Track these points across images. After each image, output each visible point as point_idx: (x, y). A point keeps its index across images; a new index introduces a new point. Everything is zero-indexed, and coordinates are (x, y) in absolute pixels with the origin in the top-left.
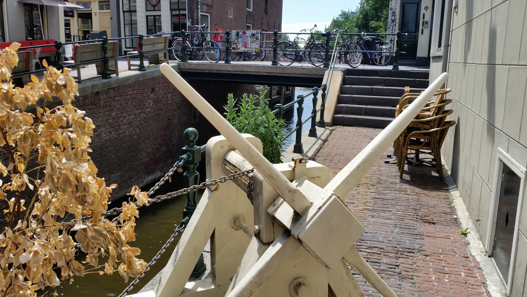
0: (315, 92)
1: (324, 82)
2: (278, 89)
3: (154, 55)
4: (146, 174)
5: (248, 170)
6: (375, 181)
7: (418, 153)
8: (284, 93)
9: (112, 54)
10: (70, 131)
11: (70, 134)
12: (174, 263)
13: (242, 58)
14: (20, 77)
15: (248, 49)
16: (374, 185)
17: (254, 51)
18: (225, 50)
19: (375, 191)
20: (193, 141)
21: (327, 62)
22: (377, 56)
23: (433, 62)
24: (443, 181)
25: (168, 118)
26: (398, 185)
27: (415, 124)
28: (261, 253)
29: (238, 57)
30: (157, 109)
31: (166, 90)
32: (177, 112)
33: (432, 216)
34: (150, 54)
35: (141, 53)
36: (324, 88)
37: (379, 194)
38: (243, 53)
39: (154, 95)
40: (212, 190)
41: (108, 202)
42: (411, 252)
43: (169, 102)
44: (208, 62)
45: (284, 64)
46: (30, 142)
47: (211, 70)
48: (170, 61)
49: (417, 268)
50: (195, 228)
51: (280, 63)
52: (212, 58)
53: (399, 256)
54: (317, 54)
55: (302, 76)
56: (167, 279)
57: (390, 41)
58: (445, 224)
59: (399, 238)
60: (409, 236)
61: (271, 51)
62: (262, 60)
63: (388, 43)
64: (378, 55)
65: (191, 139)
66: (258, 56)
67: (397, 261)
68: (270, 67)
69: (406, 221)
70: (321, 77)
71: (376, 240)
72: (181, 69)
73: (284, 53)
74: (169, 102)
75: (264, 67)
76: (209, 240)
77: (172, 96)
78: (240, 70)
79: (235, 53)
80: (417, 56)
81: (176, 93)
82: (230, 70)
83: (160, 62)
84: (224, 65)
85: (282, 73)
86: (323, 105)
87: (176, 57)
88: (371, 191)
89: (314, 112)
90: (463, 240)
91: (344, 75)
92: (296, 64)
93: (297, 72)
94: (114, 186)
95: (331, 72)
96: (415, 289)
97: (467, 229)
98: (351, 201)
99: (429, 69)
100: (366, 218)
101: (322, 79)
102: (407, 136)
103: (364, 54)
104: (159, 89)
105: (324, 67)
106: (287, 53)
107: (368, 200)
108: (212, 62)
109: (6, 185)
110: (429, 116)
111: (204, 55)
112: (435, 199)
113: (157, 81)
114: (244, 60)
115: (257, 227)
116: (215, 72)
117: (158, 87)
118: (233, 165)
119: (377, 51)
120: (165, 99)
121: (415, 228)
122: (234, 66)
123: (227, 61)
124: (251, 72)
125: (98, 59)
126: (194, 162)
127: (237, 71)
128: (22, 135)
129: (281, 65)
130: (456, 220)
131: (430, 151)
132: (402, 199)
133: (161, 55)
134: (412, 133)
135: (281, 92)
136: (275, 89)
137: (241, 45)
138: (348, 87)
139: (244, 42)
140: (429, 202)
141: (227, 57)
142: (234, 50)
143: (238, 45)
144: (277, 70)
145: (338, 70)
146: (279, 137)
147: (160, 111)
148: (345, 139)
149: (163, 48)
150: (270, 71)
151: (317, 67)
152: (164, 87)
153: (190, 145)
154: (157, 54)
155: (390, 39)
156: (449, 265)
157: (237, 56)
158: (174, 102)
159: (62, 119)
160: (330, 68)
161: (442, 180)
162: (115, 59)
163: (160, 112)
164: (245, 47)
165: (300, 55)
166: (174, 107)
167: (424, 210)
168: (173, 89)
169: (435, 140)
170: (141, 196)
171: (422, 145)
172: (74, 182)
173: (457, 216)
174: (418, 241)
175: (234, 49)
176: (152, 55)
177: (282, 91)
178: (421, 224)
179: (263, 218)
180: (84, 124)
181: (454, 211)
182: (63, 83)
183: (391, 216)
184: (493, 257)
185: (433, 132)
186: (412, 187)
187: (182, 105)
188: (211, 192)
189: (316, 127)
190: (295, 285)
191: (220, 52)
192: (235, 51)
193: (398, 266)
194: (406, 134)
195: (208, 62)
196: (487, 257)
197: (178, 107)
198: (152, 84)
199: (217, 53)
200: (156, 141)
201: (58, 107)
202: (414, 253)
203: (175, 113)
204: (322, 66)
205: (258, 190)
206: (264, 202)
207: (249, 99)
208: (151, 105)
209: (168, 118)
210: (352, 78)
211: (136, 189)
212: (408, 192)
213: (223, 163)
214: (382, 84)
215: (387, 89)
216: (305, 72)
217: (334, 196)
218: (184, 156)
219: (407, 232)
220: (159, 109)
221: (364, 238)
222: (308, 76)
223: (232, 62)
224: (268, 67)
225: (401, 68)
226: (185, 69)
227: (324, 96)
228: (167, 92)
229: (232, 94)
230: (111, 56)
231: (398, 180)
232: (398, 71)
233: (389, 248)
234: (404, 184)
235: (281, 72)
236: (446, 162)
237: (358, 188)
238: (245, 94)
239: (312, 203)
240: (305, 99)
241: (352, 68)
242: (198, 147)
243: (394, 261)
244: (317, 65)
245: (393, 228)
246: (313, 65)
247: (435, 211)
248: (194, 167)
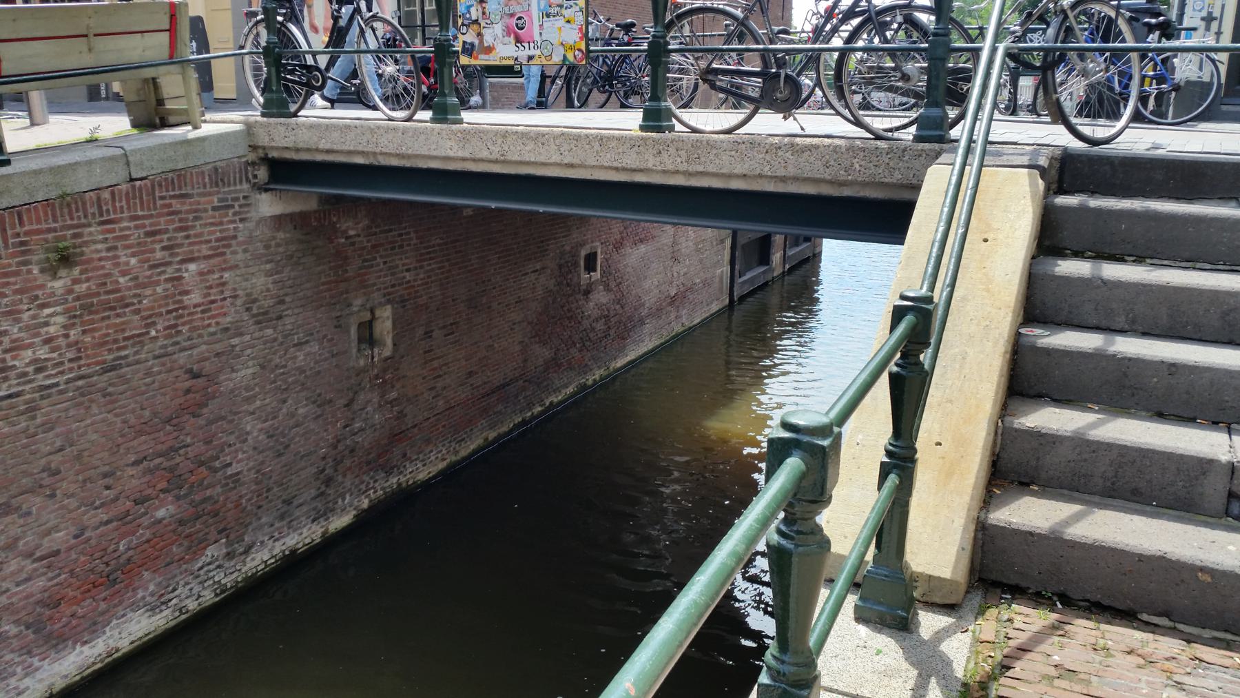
4: (36, 651)
15: (532, 52)
21: (935, 112)
43: (195, 298)
47: (375, 154)
51: (868, 120)
54: (880, 69)
55: (792, 188)
57: (1203, 19)
63: (1194, 29)
70: (906, 195)
72: (264, 148)
73: (703, 64)
75: (602, 140)
78: (493, 157)
82: (451, 154)
92: (768, 123)
93: (767, 170)
105: (918, 139)
113: (95, 210)
120: (159, 289)
124: (544, 164)
127: (482, 160)
137: (498, 29)
139: (512, 15)
142: (471, 55)
143: (483, 31)
144: (665, 155)
145: (1004, 160)
149: (164, 54)
150: (631, 160)
155: (1204, 14)
163: (123, 353)
164: (518, 40)
165: (787, 76)
175: (469, 50)
192: (473, 62)
197: (254, 316)
200: (108, 488)
203: (235, 341)
209: (190, 371)
223: (466, 116)
226: (277, 148)
246: (858, 123)
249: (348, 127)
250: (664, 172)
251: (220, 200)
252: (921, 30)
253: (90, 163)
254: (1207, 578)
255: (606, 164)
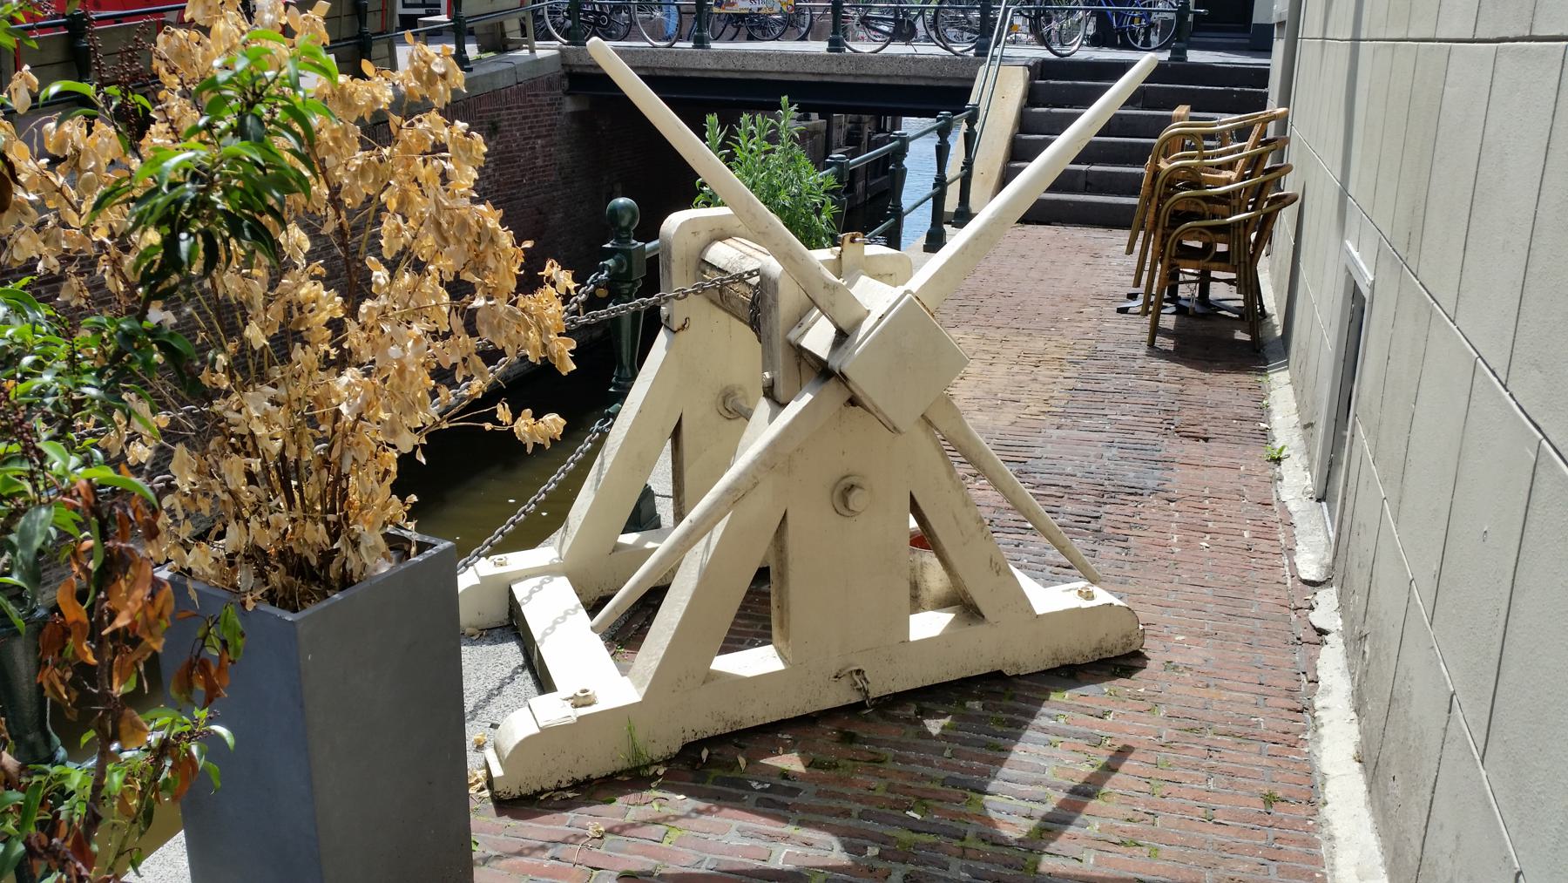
0: (943, 125)
1: (973, 100)
2: (849, 126)
3: (492, 25)
5: (750, 270)
6: (1083, 352)
7: (1205, 281)
8: (870, 137)
9: (380, 26)
10: (443, 158)
11: (443, 162)
12: (597, 484)
13: (744, 31)
14: (501, 19)
15: (761, 6)
16: (1077, 363)
17: (776, 10)
18: (694, 9)
19: (1076, 375)
20: (627, 229)
22: (1137, 20)
23: (1278, 38)
24: (1258, 351)
25: (537, 209)
26: (1139, 361)
27: (1192, 202)
28: (772, 419)
29: (731, 30)
30: (506, 184)
31: (529, 128)
32: (560, 193)
33: (1205, 426)
34: (480, 22)
35: (459, 20)
36: (970, 115)
37: (1086, 380)
38: (746, 15)
39: (498, 143)
40: (675, 329)
41: (520, 270)
42: (1135, 494)
44: (647, 44)
45: (864, 47)
46: (372, 177)
47: (653, 68)
48: (537, 43)
49: (1143, 522)
50: (640, 411)
51: (851, 46)
52: (657, 32)
53: (1105, 500)
54: (957, 18)
56: (582, 518)
58: (1233, 441)
59: (1112, 467)
60: (1139, 463)
61: (826, 9)
62: (803, 38)
64: (1141, 17)
65: (624, 223)
66: (790, 25)
67: (1098, 509)
68: (823, 56)
69: (1138, 435)
71: (1056, 471)
72: (570, 66)
74: (539, 162)
75: (806, 57)
76: (669, 441)
77: (546, 146)
78: (736, 68)
79: (722, 17)
80: (1254, 22)
81: (558, 138)
82: (709, 67)
83: (510, 46)
84: (691, 53)
85: (856, 76)
86: (968, 165)
87: (553, 31)
88: (1066, 375)
89: (941, 183)
90: (1270, 473)
91: (1032, 77)
92: (897, 49)
94: (528, 244)
95: (993, 69)
96: (1127, 558)
97: (1283, 447)
98: (1013, 397)
99: (1270, 57)
100: (1043, 430)
101: (970, 90)
102: (1169, 236)
103: (1102, 18)
104: (510, 125)
105: (976, 55)
106: (874, 13)
107: (1055, 394)
108: (655, 43)
109: (314, 264)
110: (1229, 182)
111: (632, 23)
112: (1225, 390)
114: (751, 38)
115: (767, 375)
116: (667, 73)
117: (508, 120)
118: (720, 270)
119: (1137, 5)
121: (1158, 448)
122: (721, 55)
123: (700, 42)
124: (770, 72)
125: (345, 40)
126: (631, 276)
127: (729, 71)
128: (358, 165)
129: (855, 51)
130: (1264, 433)
131: (1233, 276)
132: (1140, 390)
133: (512, 27)
134: (1183, 227)
135: (857, 134)
136: (841, 127)
138: (1042, 113)
140: (1208, 397)
141: (700, 30)
146: (823, 217)
147: (513, 188)
148: (1023, 256)
150: (823, 68)
151: (956, 55)
152: (524, 118)
153: (621, 238)
154: (502, 24)
156: (1219, 518)
157: (729, 26)
158: (553, 162)
159: (426, 139)
160: (989, 58)
161: (1257, 348)
162: (388, 40)
165: (909, 21)
166: (553, 178)
167: (1190, 413)
168: (550, 125)
169: (1242, 243)
170: (562, 277)
171: (1209, 258)
172: (475, 228)
173: (1269, 424)
174: (1157, 473)
176: (486, 27)
177: (862, 133)
178: (1172, 440)
179: (780, 354)
180: (470, 144)
181: (1265, 413)
182: (443, 70)
183: (1102, 426)
184: (1324, 500)
185: (1238, 222)
186: (1173, 365)
187: (573, 172)
188: (672, 334)
189: (947, 227)
190: (843, 488)
191: (680, 13)
192: (722, 11)
193: (1097, 517)
194: (1169, 231)
195: (647, 44)
196: (1313, 502)
198: (490, 111)
199: (669, 16)
201: (417, 117)
202: (1142, 495)
203: (555, 194)
204: (971, 54)
205: (769, 300)
206: (781, 322)
207: (755, 126)
208: (489, 171)
210: (1053, 85)
211: (552, 266)
212: (1161, 377)
213: (699, 268)
214: (1139, 101)
215: (1149, 116)
216: (924, 70)
217: (908, 296)
218: (610, 262)
219: (1135, 456)
220: (511, 183)
221: (1030, 469)
222: (931, 83)
223: (715, 46)
224: (818, 57)
225: (1194, 56)
226: (580, 66)
227: (970, 139)
228: (533, 132)
229: (716, 115)
230: (379, 30)
231: (1142, 351)
232: (1184, 65)
233: (1084, 486)
234: (1154, 359)
235: (854, 72)
236: (1271, 300)
237: (1035, 369)
238: (745, 115)
239: (869, 312)
240: (912, 145)
241: (1055, 57)
242: (640, 244)
243: (1090, 510)
244: (957, 49)
245: (1105, 449)
246: (947, 48)
247: (1216, 414)
248: (631, 290)
249: (637, 51)
250: (842, 75)
251: (551, 100)
252: (782, 565)
253: (503, 71)
254: (1071, 205)
255: (808, 71)
